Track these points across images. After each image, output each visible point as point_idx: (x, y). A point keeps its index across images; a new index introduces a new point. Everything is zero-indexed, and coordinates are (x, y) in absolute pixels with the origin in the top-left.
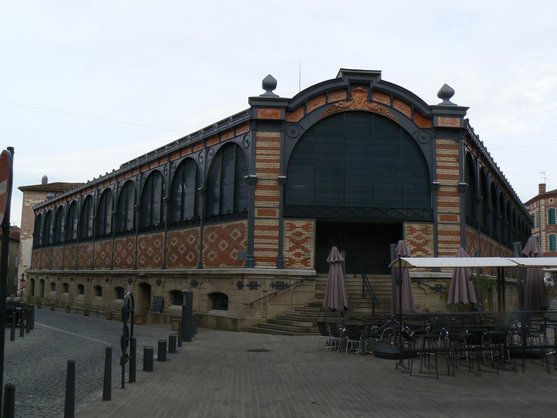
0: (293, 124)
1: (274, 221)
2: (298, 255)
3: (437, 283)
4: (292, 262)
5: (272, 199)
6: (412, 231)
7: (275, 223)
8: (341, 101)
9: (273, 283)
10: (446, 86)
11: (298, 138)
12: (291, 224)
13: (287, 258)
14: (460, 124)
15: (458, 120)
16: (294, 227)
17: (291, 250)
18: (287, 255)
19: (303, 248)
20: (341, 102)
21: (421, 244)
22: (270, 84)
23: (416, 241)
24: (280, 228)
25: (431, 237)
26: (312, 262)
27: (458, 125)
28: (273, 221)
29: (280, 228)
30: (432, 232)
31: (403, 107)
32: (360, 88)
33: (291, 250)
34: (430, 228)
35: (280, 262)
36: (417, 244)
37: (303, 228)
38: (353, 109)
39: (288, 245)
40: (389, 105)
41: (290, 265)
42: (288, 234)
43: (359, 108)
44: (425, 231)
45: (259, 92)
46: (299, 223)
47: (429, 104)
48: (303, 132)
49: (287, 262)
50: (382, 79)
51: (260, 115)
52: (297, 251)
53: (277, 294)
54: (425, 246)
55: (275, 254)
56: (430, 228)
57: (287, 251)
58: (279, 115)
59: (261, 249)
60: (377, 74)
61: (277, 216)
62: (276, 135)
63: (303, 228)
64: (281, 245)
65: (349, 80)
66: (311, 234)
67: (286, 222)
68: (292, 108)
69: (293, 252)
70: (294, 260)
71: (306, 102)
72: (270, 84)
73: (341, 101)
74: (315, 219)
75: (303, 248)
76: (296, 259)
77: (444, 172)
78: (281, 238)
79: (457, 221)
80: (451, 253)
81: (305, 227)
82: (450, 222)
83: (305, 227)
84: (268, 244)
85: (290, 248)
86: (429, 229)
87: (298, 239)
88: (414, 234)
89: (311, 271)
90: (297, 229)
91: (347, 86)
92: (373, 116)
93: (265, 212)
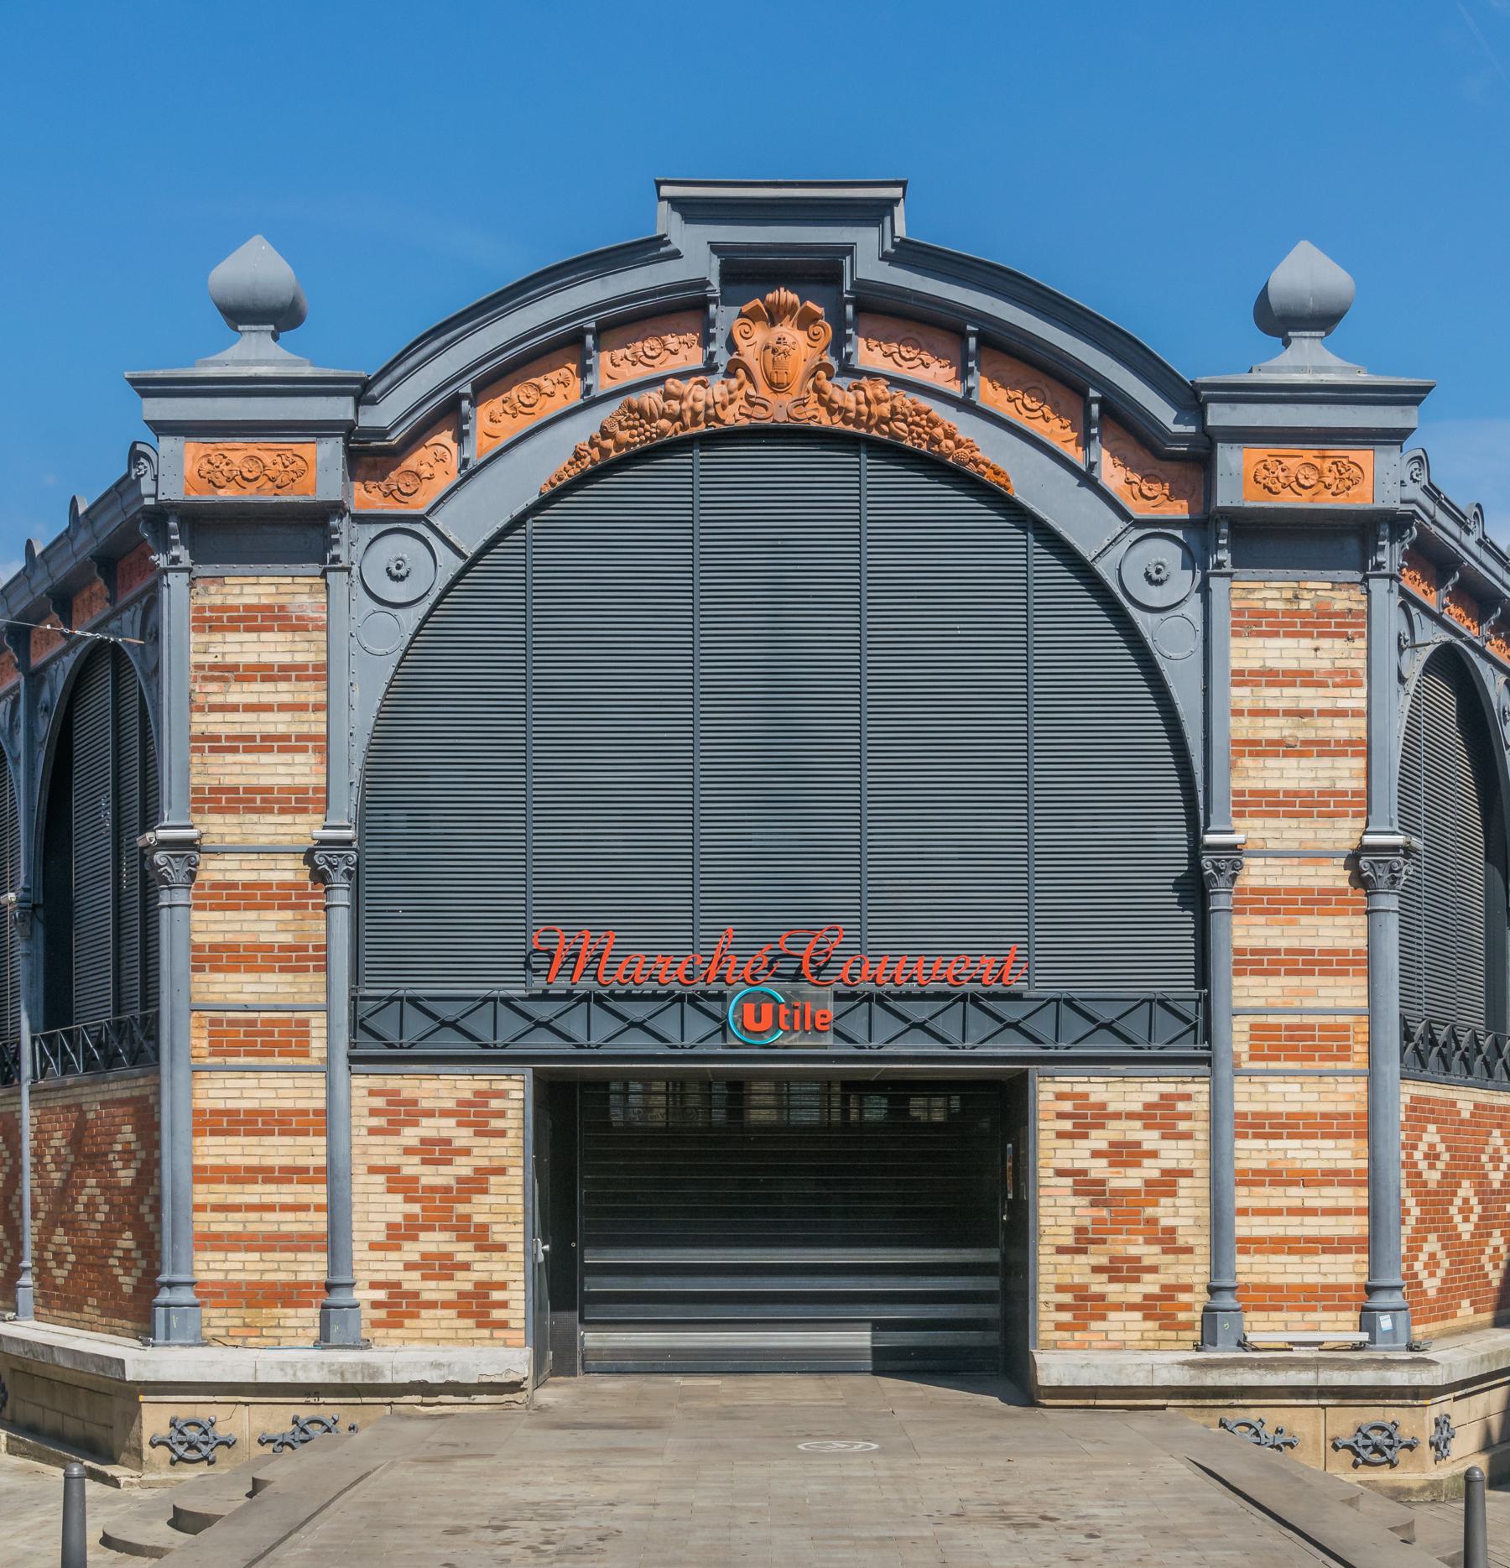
0: (396, 525)
1: (303, 1081)
3: (185, 1413)
5: (290, 959)
6: (1086, 1119)
7: (1348, 1096)
8: (675, 376)
11: (423, 608)
12: (392, 1096)
16: (1100, 1116)
19: (466, 1230)
20: (673, 385)
26: (516, 1301)
30: (1200, 1127)
32: (786, 296)
34: (1187, 1097)
37: (1148, 1116)
38: (745, 422)
42: (386, 1151)
43: (781, 418)
44: (1160, 1116)
48: (450, 564)
54: (1156, 1205)
59: (288, 1236)
63: (1148, 1116)
64: (337, 1209)
65: (715, 248)
68: (382, 433)
69: (411, 1252)
70: (1101, 1297)
71: (467, 389)
73: (675, 376)
74: (528, 1070)
75: (466, 1230)
77: (237, 769)
81: (476, 1115)
87: (432, 1177)
88: (1094, 1133)
91: (703, 283)
92: (863, 448)
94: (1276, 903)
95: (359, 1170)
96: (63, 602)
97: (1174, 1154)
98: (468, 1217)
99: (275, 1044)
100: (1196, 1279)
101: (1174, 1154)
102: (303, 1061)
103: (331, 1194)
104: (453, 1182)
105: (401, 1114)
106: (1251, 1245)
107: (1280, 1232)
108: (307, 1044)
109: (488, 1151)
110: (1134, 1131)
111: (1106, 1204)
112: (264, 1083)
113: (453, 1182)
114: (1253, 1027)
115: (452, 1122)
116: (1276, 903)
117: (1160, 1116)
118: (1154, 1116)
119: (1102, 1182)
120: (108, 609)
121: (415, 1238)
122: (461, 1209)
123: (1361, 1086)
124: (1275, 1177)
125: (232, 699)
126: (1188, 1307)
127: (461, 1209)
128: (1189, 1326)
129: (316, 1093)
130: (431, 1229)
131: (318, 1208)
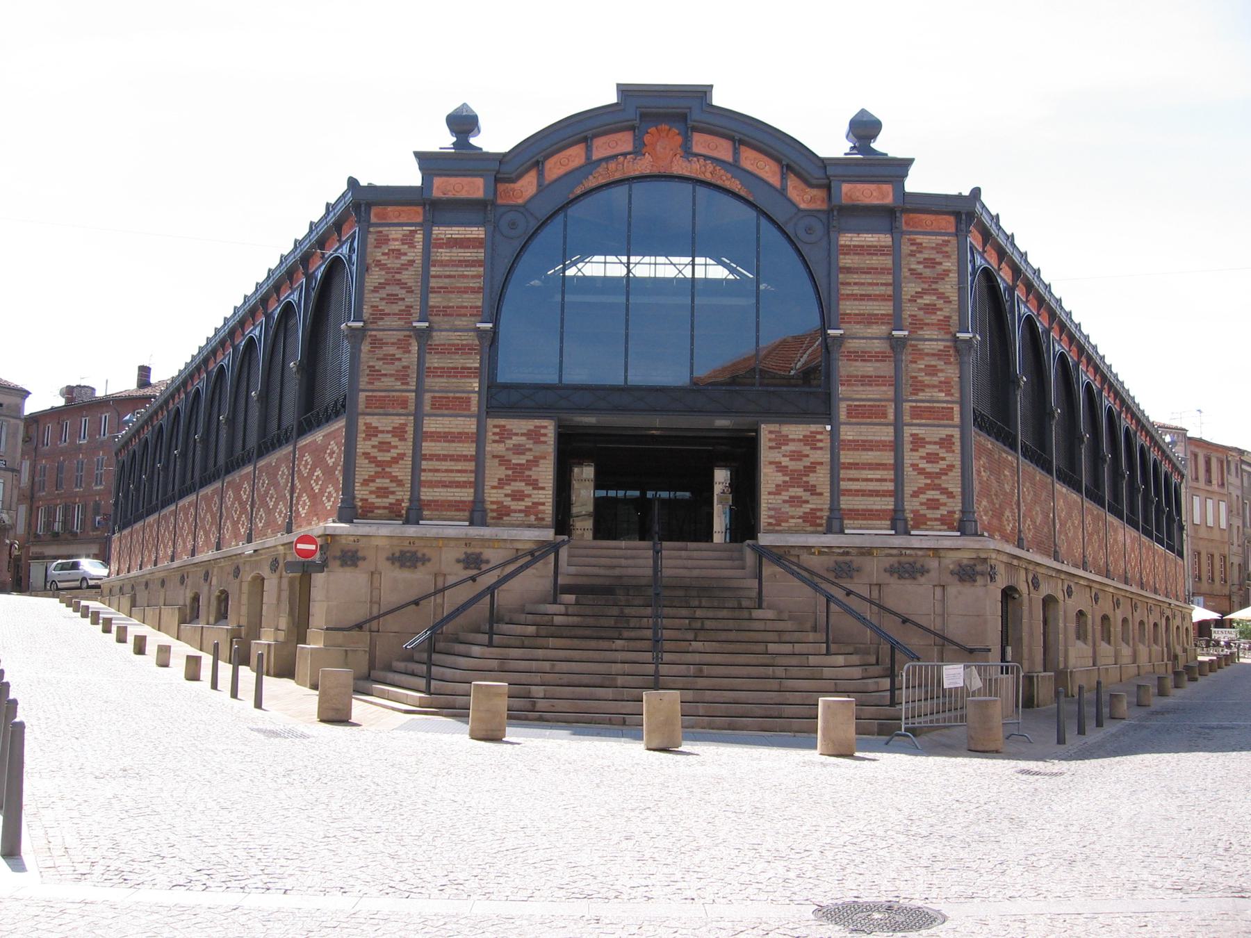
2: (517, 496)
4: (920, 522)
6: (782, 441)
9: (393, 554)
10: (863, 112)
13: (492, 503)
14: (485, 192)
15: (888, 188)
16: (786, 440)
17: (502, 483)
18: (493, 496)
21: (801, 471)
22: (463, 123)
23: (377, 454)
24: (479, 438)
25: (823, 456)
27: (889, 200)
28: (873, 430)
29: (479, 438)
31: (761, 164)
33: (502, 483)
34: (545, 427)
35: (898, 522)
36: (791, 471)
39: (494, 472)
40: (731, 160)
41: (500, 517)
42: (499, 449)
44: (810, 441)
45: (442, 140)
46: (520, 426)
47: (821, 154)
49: (492, 511)
50: (714, 103)
51: (444, 187)
52: (793, 494)
53: (851, 596)
55: (467, 495)
56: (545, 427)
57: (494, 487)
58: (474, 188)
60: (703, 93)
61: (474, 408)
62: (477, 232)
64: (479, 472)
66: (549, 447)
67: (491, 422)
72: (463, 123)
76: (930, 514)
78: (479, 459)
79: (953, 420)
80: (851, 490)
81: (535, 435)
82: (942, 422)
83: (535, 435)
84: (877, 480)
85: (777, 486)
86: (543, 431)
89: (549, 534)
90: (380, 435)
93: (861, 413)
94: (863, 356)
95: (488, 456)
96: (321, 243)
97: (817, 456)
98: (808, 482)
99: (443, 405)
100: (956, 509)
101: (817, 456)
102: (950, 422)
103: (896, 475)
104: (802, 468)
105: (504, 435)
106: (849, 492)
107: (858, 487)
108: (470, 406)
109: (539, 449)
110: (388, 437)
111: (510, 469)
112: (870, 430)
113: (802, 468)
114: (848, 406)
115: (390, 435)
116: (863, 356)
117: (810, 441)
118: (944, 443)
119: (787, 467)
120: (338, 244)
121: (509, 484)
122: (527, 473)
123: (891, 429)
124: (855, 466)
125: (447, 280)
126: (821, 518)
127: (527, 473)
128: (821, 525)
129: (472, 426)
130: (516, 480)
131: (471, 471)
